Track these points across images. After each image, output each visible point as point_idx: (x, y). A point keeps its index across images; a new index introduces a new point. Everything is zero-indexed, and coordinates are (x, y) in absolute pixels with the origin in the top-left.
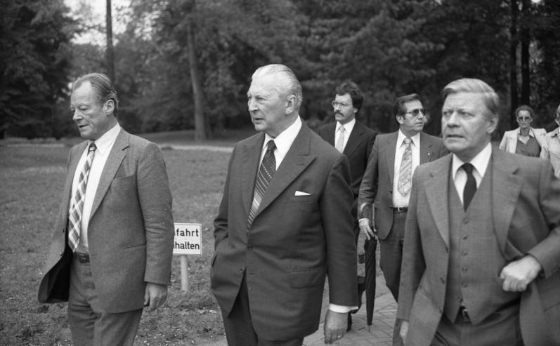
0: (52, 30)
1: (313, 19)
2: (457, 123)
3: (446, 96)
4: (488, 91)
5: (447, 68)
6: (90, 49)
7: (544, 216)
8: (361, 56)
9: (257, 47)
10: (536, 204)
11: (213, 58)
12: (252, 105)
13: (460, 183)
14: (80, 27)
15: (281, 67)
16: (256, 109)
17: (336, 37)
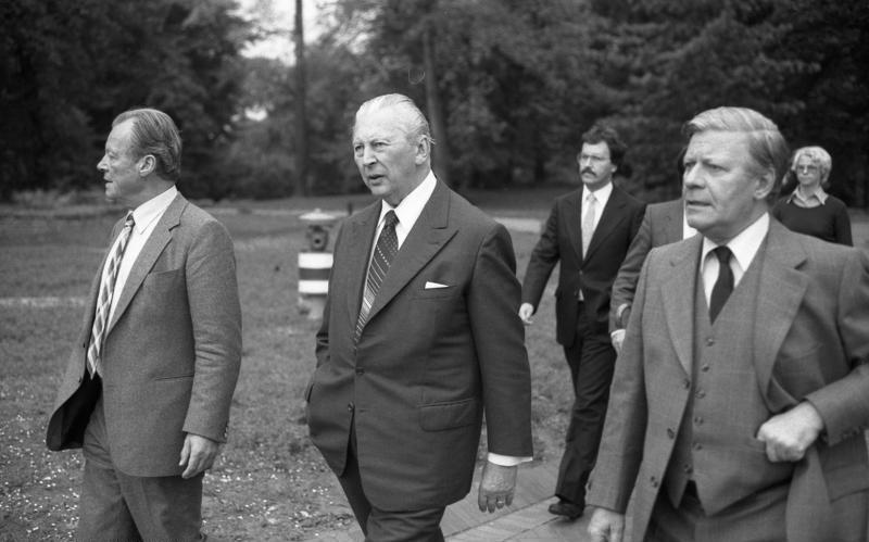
0: (212, 36)
1: (617, 21)
2: (699, 182)
3: (691, 136)
4: (759, 127)
5: (822, 100)
6: (263, 66)
7: (843, 343)
8: (692, 81)
9: (528, 65)
10: (830, 323)
11: (462, 81)
12: (364, 158)
13: (711, 275)
14: (254, 31)
15: (399, 97)
16: (374, 160)
17: (653, 51)
